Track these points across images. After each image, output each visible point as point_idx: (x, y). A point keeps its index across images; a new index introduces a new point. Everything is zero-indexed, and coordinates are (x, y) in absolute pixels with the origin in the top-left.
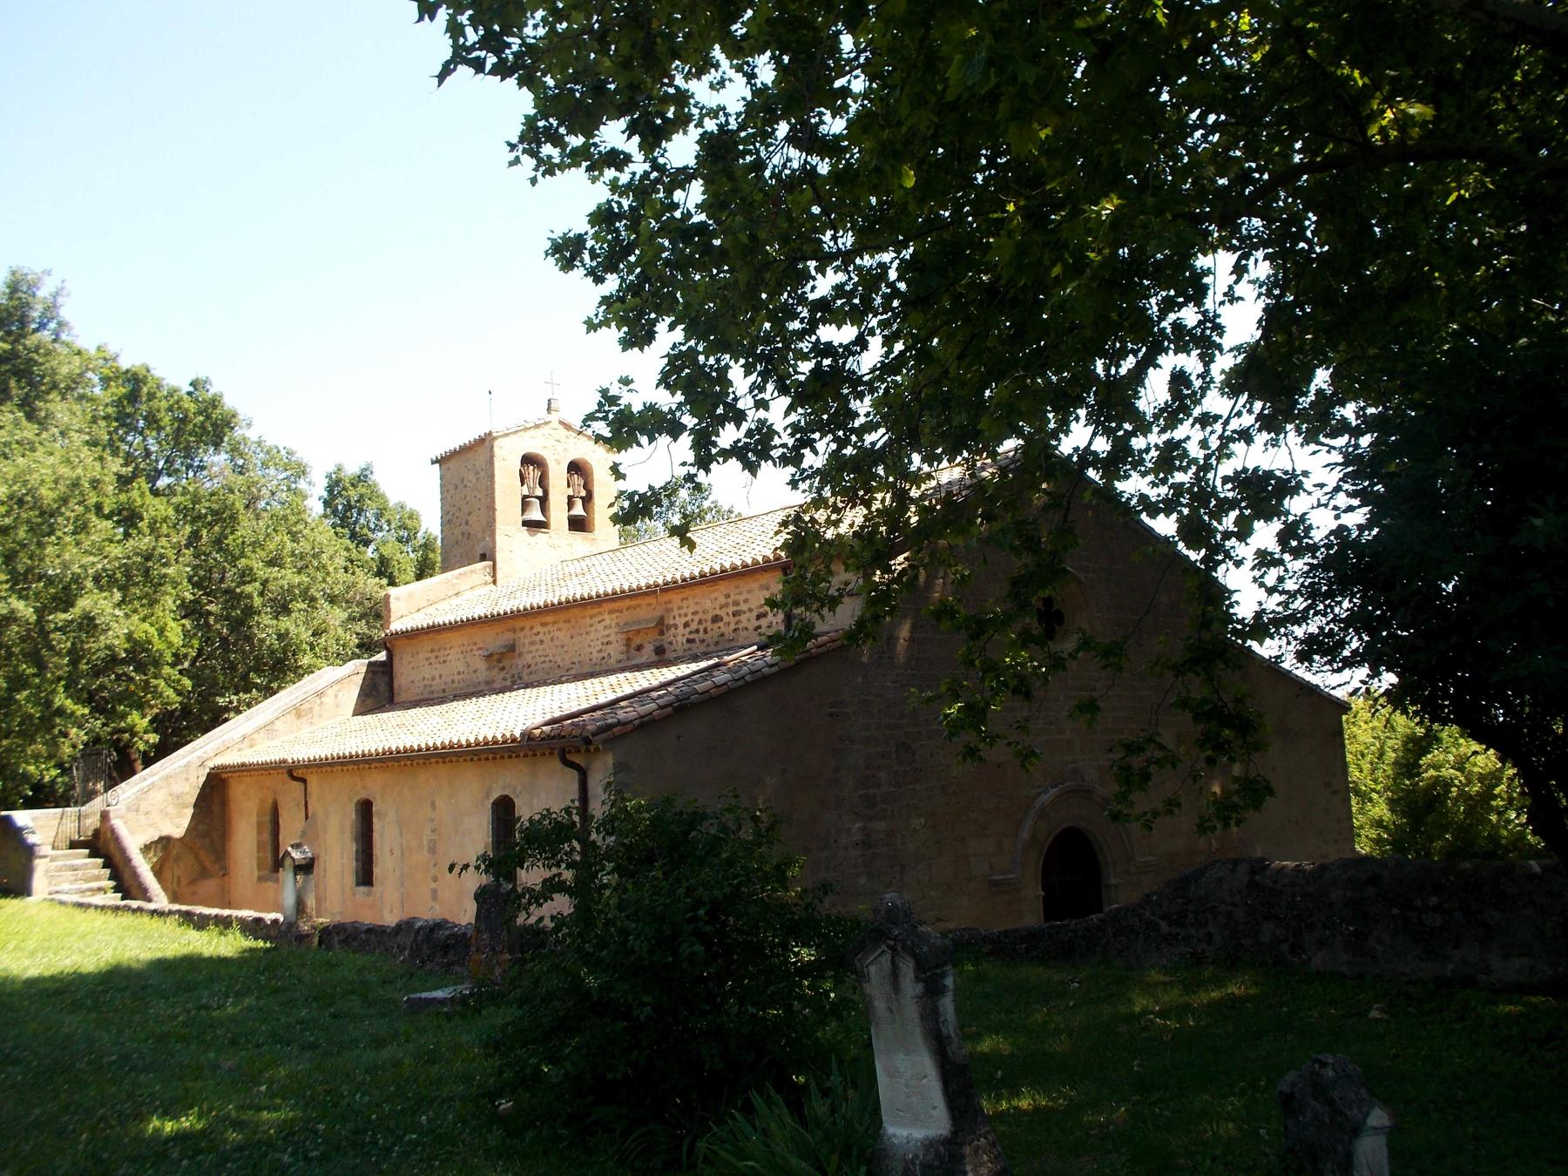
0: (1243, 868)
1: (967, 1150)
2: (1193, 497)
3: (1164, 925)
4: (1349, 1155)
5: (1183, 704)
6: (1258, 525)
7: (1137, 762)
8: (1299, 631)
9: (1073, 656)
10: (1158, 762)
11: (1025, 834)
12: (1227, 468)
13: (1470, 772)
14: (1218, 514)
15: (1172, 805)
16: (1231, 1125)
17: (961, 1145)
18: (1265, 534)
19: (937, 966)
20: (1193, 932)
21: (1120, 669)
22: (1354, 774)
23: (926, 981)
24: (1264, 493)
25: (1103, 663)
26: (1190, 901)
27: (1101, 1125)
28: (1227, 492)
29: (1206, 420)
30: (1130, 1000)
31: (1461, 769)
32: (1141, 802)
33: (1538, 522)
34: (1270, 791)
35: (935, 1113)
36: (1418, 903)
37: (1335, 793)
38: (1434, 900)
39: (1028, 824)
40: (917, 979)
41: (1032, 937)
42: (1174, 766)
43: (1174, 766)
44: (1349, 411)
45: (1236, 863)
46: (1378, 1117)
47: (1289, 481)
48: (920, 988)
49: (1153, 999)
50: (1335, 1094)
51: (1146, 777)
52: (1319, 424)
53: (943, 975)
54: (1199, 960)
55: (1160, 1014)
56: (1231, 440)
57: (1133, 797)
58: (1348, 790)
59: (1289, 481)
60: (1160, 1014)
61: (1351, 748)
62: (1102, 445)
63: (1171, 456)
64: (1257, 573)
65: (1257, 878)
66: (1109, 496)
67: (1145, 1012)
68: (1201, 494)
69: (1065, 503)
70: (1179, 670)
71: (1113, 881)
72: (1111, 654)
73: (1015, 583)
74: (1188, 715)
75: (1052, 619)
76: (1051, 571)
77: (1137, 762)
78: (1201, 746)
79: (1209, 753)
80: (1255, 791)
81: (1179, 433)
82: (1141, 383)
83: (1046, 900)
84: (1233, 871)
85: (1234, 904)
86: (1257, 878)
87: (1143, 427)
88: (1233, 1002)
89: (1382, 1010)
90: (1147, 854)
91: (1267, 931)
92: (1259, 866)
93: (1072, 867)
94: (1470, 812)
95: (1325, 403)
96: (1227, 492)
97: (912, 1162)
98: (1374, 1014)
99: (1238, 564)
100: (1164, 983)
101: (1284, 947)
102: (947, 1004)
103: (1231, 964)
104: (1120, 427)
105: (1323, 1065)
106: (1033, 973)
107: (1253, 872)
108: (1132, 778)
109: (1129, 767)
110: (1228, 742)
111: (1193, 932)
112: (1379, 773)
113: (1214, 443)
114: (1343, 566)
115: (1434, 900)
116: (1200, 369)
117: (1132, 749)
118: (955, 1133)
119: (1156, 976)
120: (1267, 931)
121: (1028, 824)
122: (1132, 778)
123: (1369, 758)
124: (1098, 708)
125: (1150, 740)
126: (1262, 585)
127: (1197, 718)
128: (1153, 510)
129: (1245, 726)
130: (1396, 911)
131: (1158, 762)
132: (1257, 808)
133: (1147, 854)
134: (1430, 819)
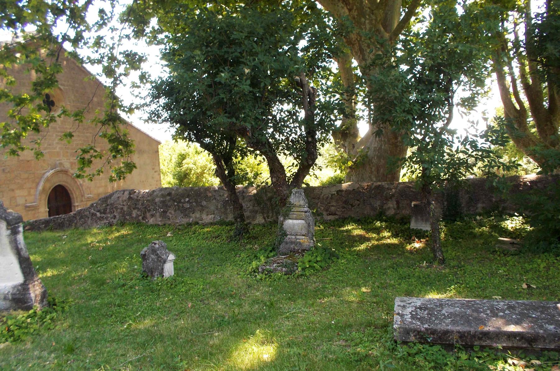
0: (126, 193)
1: (30, 286)
2: (109, 58)
3: (98, 214)
4: (163, 269)
5: (105, 136)
6: (132, 72)
7: (87, 156)
8: (147, 109)
9: (59, 116)
10: (95, 157)
11: (40, 188)
12: (122, 49)
13: (198, 166)
14: (118, 66)
15: (99, 172)
16: (124, 269)
17: (28, 285)
18: (135, 75)
19: (16, 223)
20: (109, 215)
21: (82, 121)
22: (162, 166)
23: (11, 229)
24: (134, 60)
25: (75, 119)
26: (108, 205)
27: (79, 276)
28: (121, 58)
29: (113, 29)
30: (86, 239)
31: (195, 164)
32: (88, 170)
33: (223, 75)
34: (135, 167)
35: (17, 276)
36: (183, 201)
37: (155, 172)
38: (187, 199)
39: (42, 184)
40: (8, 229)
41: (46, 223)
42: (101, 158)
43: (101, 158)
44: (161, 36)
45: (124, 191)
46: (171, 257)
47: (143, 57)
48: (9, 232)
49: (95, 237)
50: (158, 252)
51: (90, 162)
52: (154, 40)
53: (19, 227)
54: (111, 225)
55: (98, 242)
56: (122, 37)
57: (85, 169)
58: (160, 171)
59: (143, 57)
60: (98, 242)
61: (161, 158)
62: (72, 34)
63: (98, 42)
64: (132, 90)
65: (132, 196)
66: (74, 55)
67: (92, 242)
68: (112, 58)
69: (57, 54)
70: (103, 123)
71: (76, 204)
72: (78, 115)
73: (35, 84)
74: (106, 140)
75: (49, 104)
76: (51, 82)
77: (87, 156)
78: (111, 151)
79: (114, 154)
80: (130, 167)
81: (101, 33)
82: (86, 11)
83: (49, 212)
84: (123, 194)
85: (124, 205)
86: (132, 196)
87: (88, 29)
88: (123, 236)
89: (171, 233)
90: (90, 190)
91: (135, 213)
92: (132, 192)
93: (60, 199)
94: (197, 178)
95: (155, 32)
96: (121, 58)
97: (8, 294)
98: (169, 235)
99: (125, 85)
100: (99, 233)
101: (140, 218)
102: (20, 237)
103: (122, 224)
104: (78, 27)
105: (155, 244)
106: (47, 234)
107: (130, 194)
108: (85, 163)
109: (83, 159)
110: (121, 150)
111: (109, 215)
112: (170, 166)
113: (117, 38)
114: (160, 89)
115: (187, 199)
116: (111, 9)
117: (85, 151)
118: (25, 281)
119: (95, 231)
120: (135, 213)
121: (42, 184)
122: (85, 163)
123: (166, 161)
124: (73, 136)
125: (91, 149)
126: (133, 94)
127: (110, 141)
128: (92, 62)
129: (127, 145)
130: (176, 204)
131: (95, 157)
132: (130, 172)
133: (90, 190)
134: (185, 181)
